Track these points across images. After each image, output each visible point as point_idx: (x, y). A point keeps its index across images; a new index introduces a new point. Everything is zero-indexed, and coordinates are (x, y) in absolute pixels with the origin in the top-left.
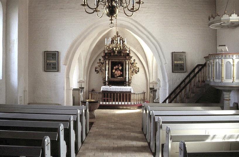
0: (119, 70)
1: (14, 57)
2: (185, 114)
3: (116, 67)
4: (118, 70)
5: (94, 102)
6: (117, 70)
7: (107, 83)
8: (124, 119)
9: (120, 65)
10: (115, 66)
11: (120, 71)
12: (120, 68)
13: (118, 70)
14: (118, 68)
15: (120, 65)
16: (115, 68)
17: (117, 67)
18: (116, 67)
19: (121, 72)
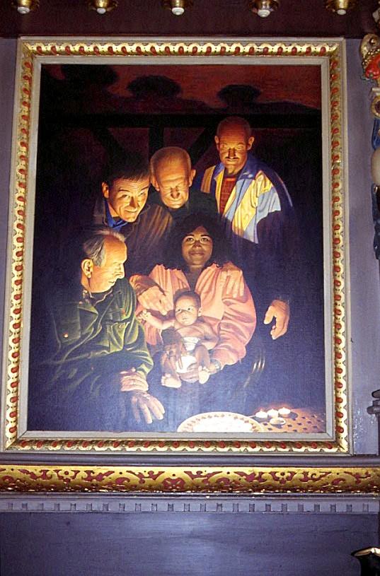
0: (227, 247)
1: (120, 195)
2: (78, 61)
3: (154, 196)
4: (197, 243)
5: (133, 488)
6: (174, 260)
7: (224, 301)
8: (317, 382)
9: (233, 147)
10: (136, 169)
11: (232, 281)
12: (251, 204)
13: (197, 243)
14: (204, 214)
15: (233, 147)
16: (130, 198)
17: (175, 185)
18: (154, 196)
19: (261, 296)
